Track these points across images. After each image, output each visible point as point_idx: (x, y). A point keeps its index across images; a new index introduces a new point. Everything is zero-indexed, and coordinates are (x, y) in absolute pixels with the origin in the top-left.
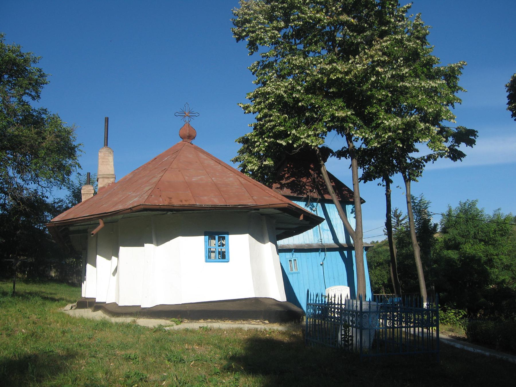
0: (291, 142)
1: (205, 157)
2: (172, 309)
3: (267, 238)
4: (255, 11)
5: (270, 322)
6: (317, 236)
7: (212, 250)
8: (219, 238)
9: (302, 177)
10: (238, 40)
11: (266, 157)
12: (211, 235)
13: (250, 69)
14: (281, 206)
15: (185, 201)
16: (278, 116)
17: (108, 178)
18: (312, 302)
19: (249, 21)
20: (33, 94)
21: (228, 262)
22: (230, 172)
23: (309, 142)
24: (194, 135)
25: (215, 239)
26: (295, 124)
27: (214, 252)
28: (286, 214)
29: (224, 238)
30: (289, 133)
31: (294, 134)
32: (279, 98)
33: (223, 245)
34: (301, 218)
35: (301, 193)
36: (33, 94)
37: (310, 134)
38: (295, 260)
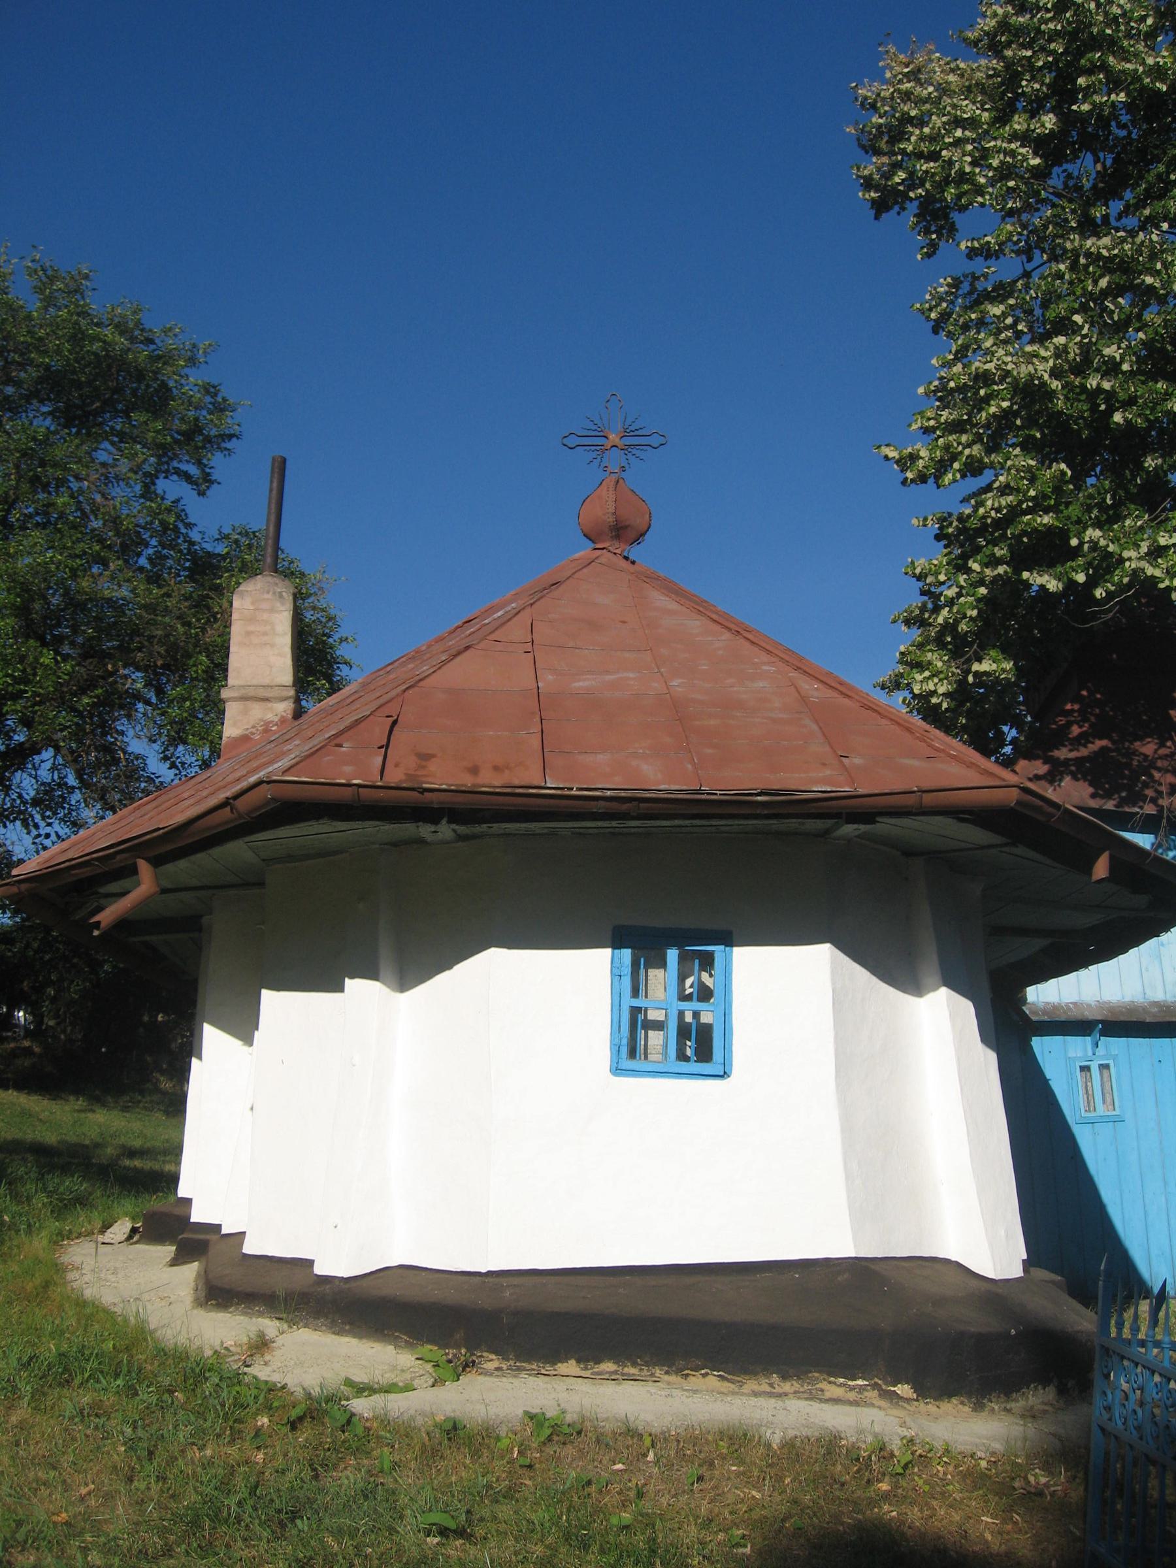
0: (1081, 578)
1: (673, 606)
2: (449, 1296)
3: (930, 967)
4: (944, 90)
5: (923, 1391)
7: (653, 1015)
8: (683, 958)
9: (1141, 739)
10: (880, 207)
11: (982, 647)
12: (642, 942)
13: (922, 311)
14: (985, 797)
15: (496, 768)
16: (1029, 469)
17: (267, 700)
19: (921, 122)
20: (193, 470)
21: (724, 1075)
22: (765, 657)
23: (1157, 573)
24: (639, 522)
25: (663, 964)
26: (1102, 506)
27: (659, 1026)
28: (1020, 850)
29: (707, 962)
30: (1074, 542)
31: (1094, 545)
32: (1031, 393)
33: (705, 994)
34: (1101, 869)
35: (1136, 798)
36: (193, 470)
37: (1162, 542)
38: (1107, 1067)
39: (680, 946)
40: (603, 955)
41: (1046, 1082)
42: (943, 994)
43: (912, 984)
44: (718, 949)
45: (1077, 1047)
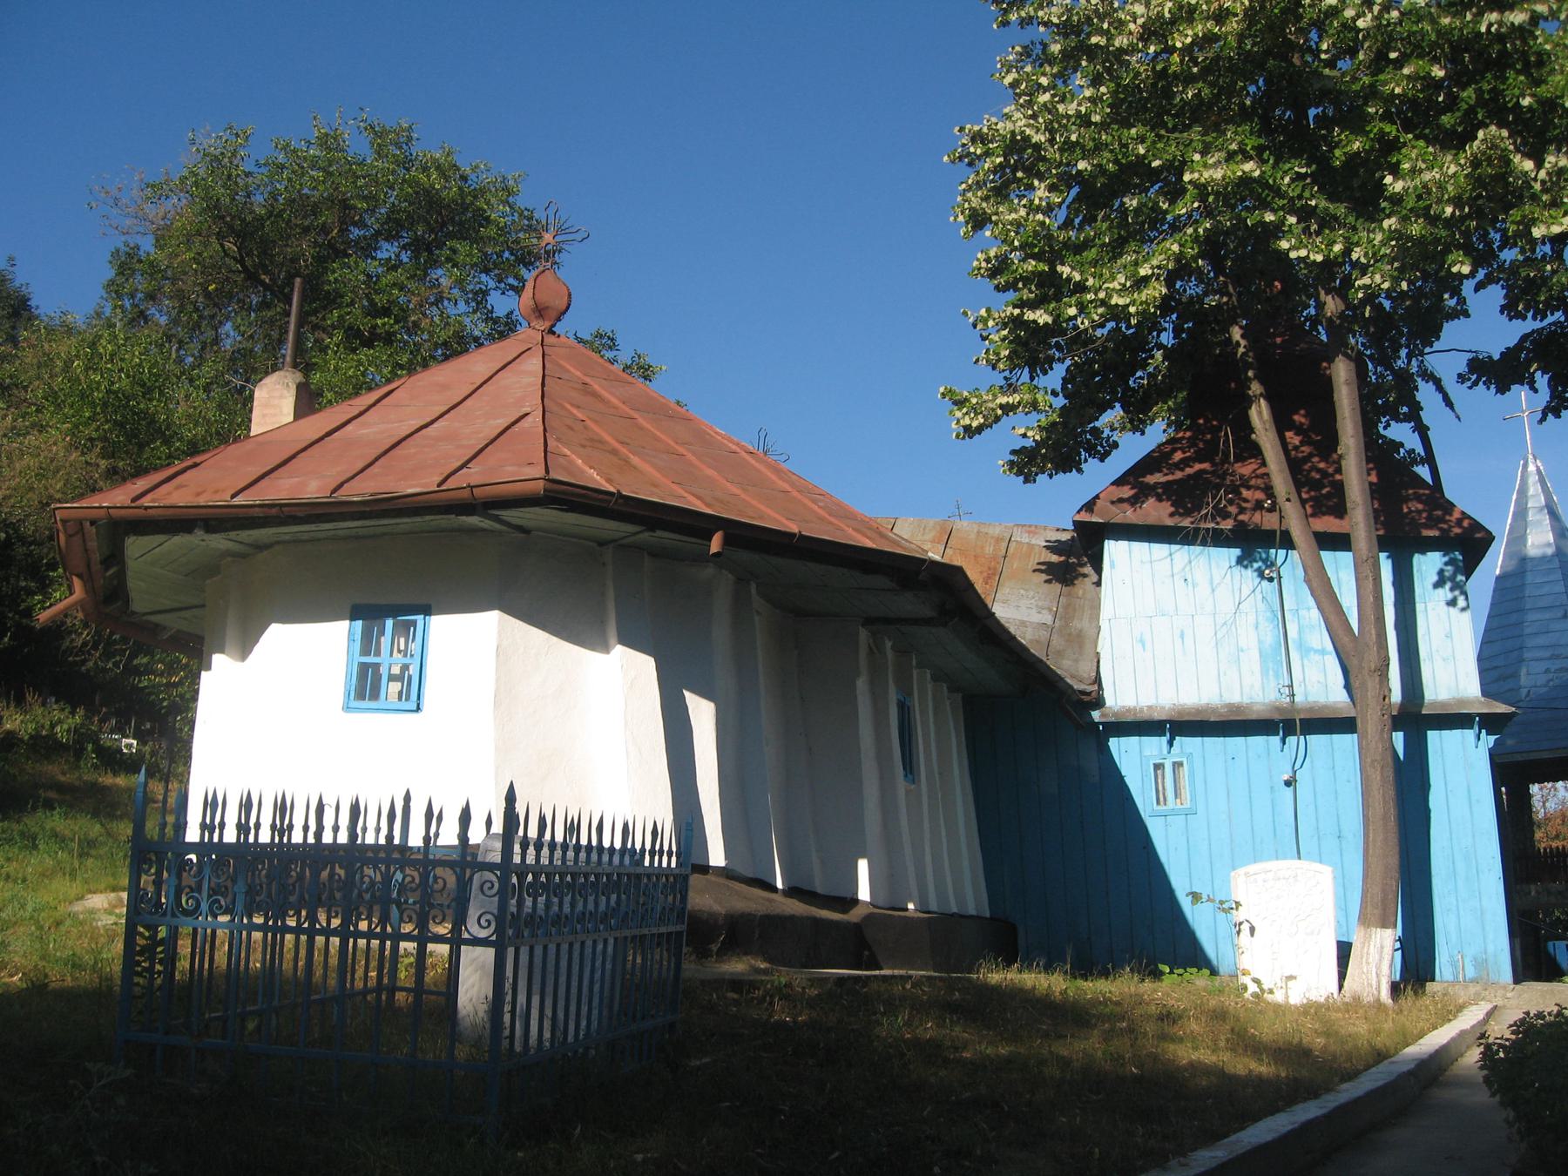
6: (1277, 676)
12: (368, 613)
18: (530, 859)
34: (715, 545)
38: (1180, 764)
39: (394, 617)
40: (343, 626)
41: (1122, 778)
42: (619, 651)
43: (606, 649)
44: (419, 618)
45: (1154, 746)
